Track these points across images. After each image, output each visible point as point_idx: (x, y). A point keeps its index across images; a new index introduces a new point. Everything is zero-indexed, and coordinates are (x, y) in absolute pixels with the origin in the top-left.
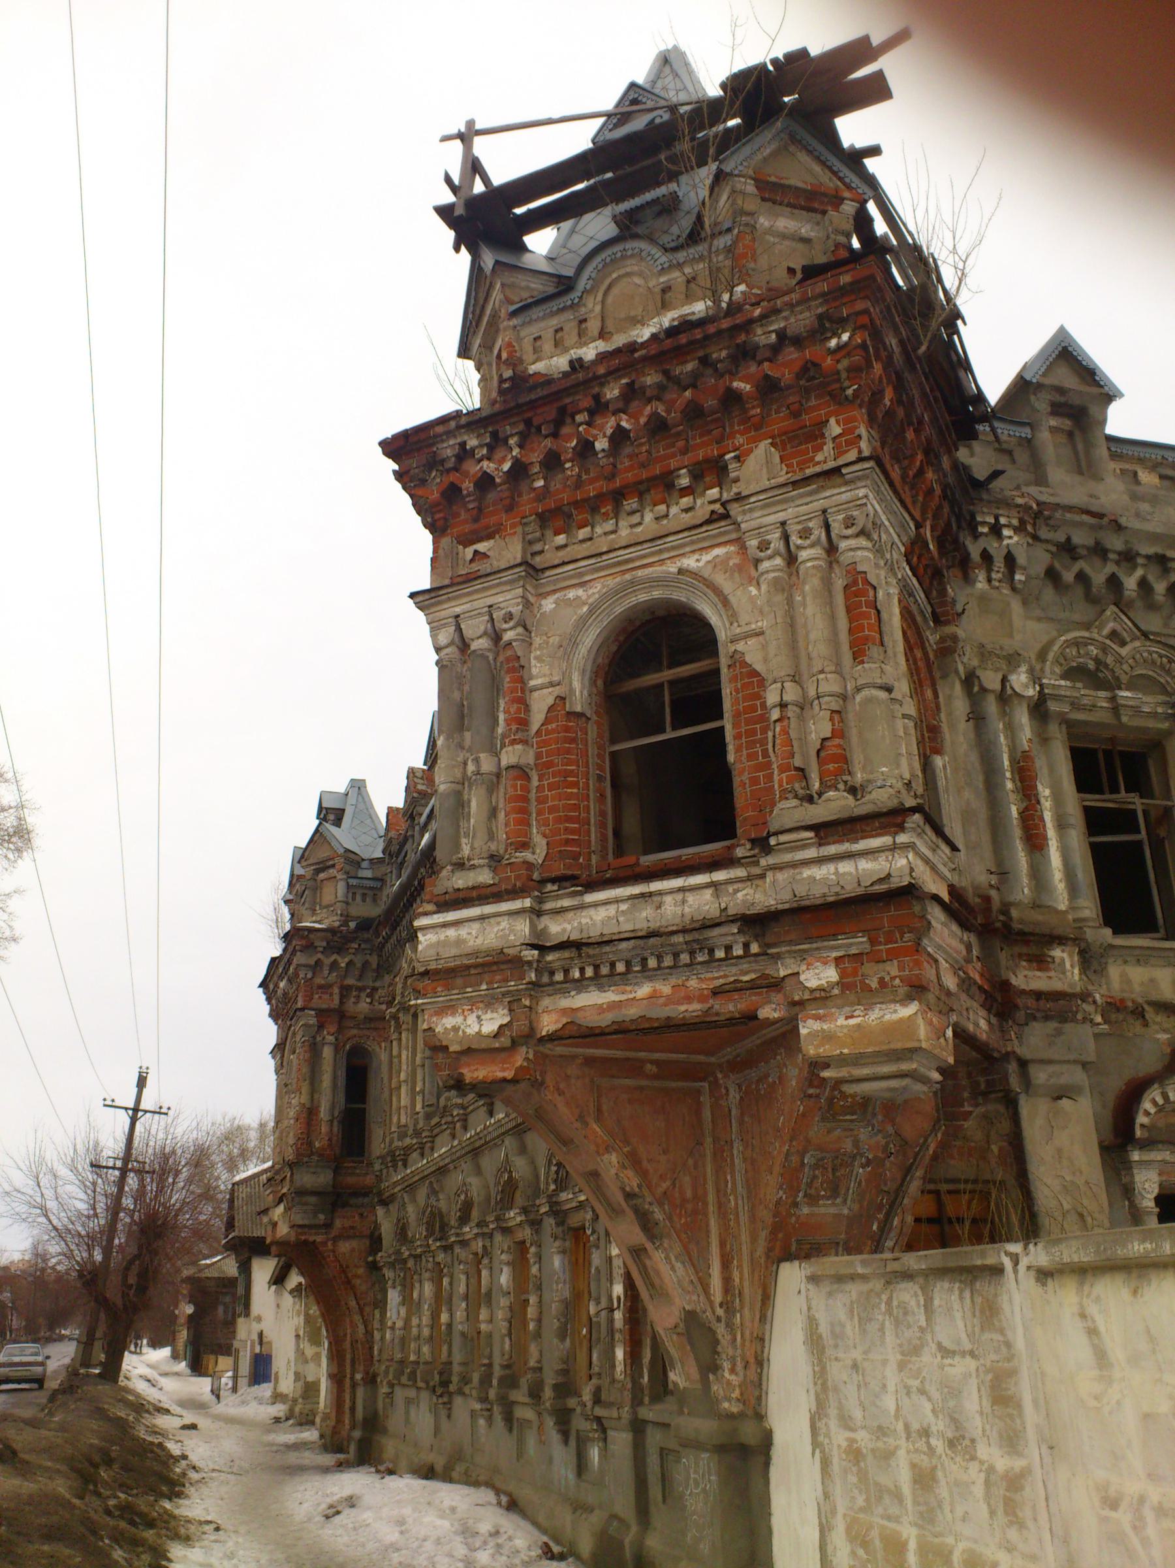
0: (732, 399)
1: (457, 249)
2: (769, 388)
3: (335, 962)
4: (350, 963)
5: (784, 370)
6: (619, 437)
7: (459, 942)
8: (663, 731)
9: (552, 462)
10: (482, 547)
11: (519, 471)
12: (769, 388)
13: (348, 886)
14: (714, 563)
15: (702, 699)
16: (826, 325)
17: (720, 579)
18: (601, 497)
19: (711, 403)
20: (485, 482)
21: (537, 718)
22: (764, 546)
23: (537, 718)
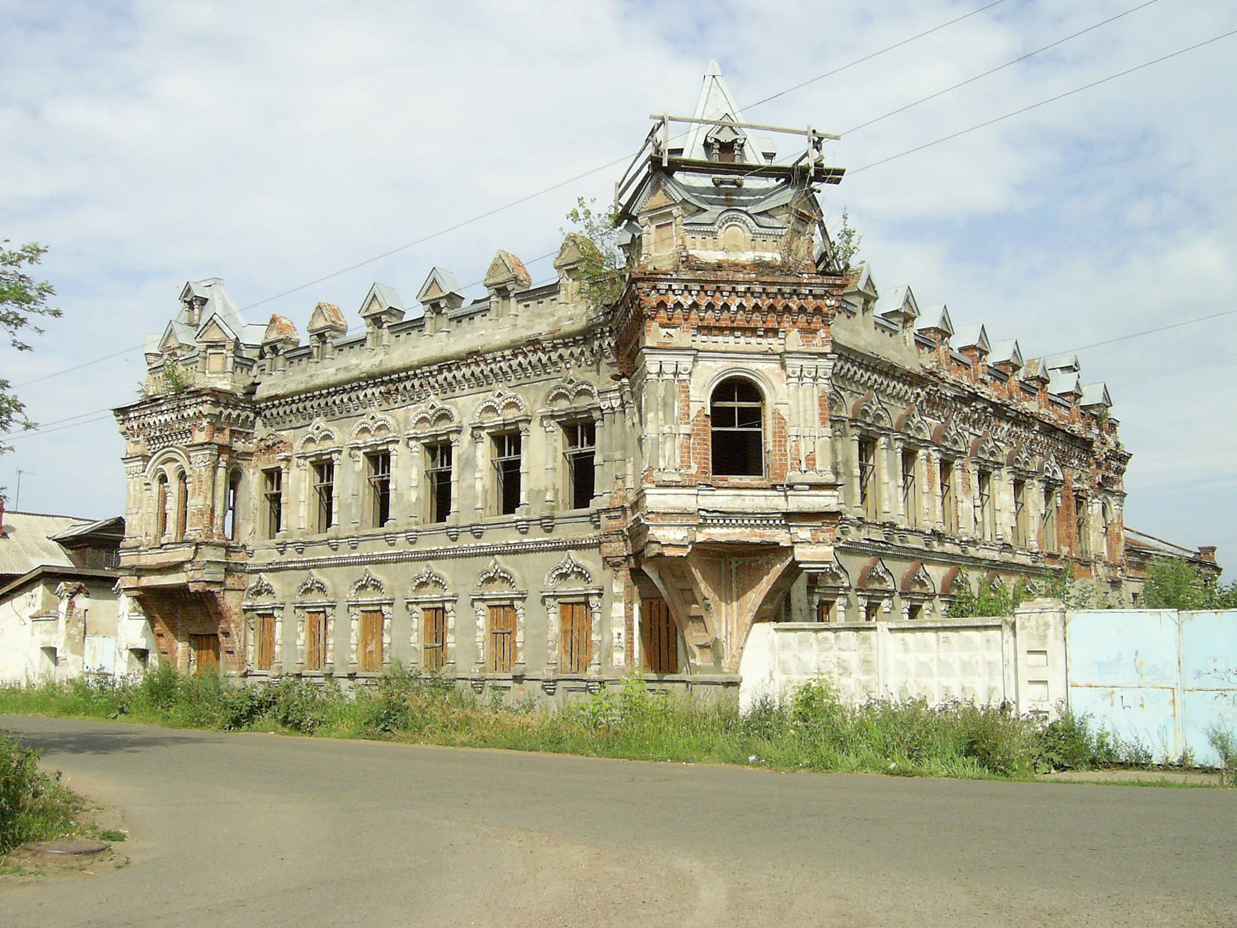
0: (787, 309)
1: (1220, 742)
2: (802, 309)
3: (230, 414)
4: (239, 415)
5: (811, 304)
6: (741, 306)
7: (665, 502)
8: (733, 425)
9: (710, 306)
10: (671, 331)
11: (695, 305)
12: (802, 309)
13: (235, 362)
14: (770, 370)
15: (754, 416)
16: (828, 294)
17: (772, 377)
18: (727, 328)
19: (780, 308)
20: (678, 305)
21: (693, 415)
22: (794, 373)
23: (693, 415)
